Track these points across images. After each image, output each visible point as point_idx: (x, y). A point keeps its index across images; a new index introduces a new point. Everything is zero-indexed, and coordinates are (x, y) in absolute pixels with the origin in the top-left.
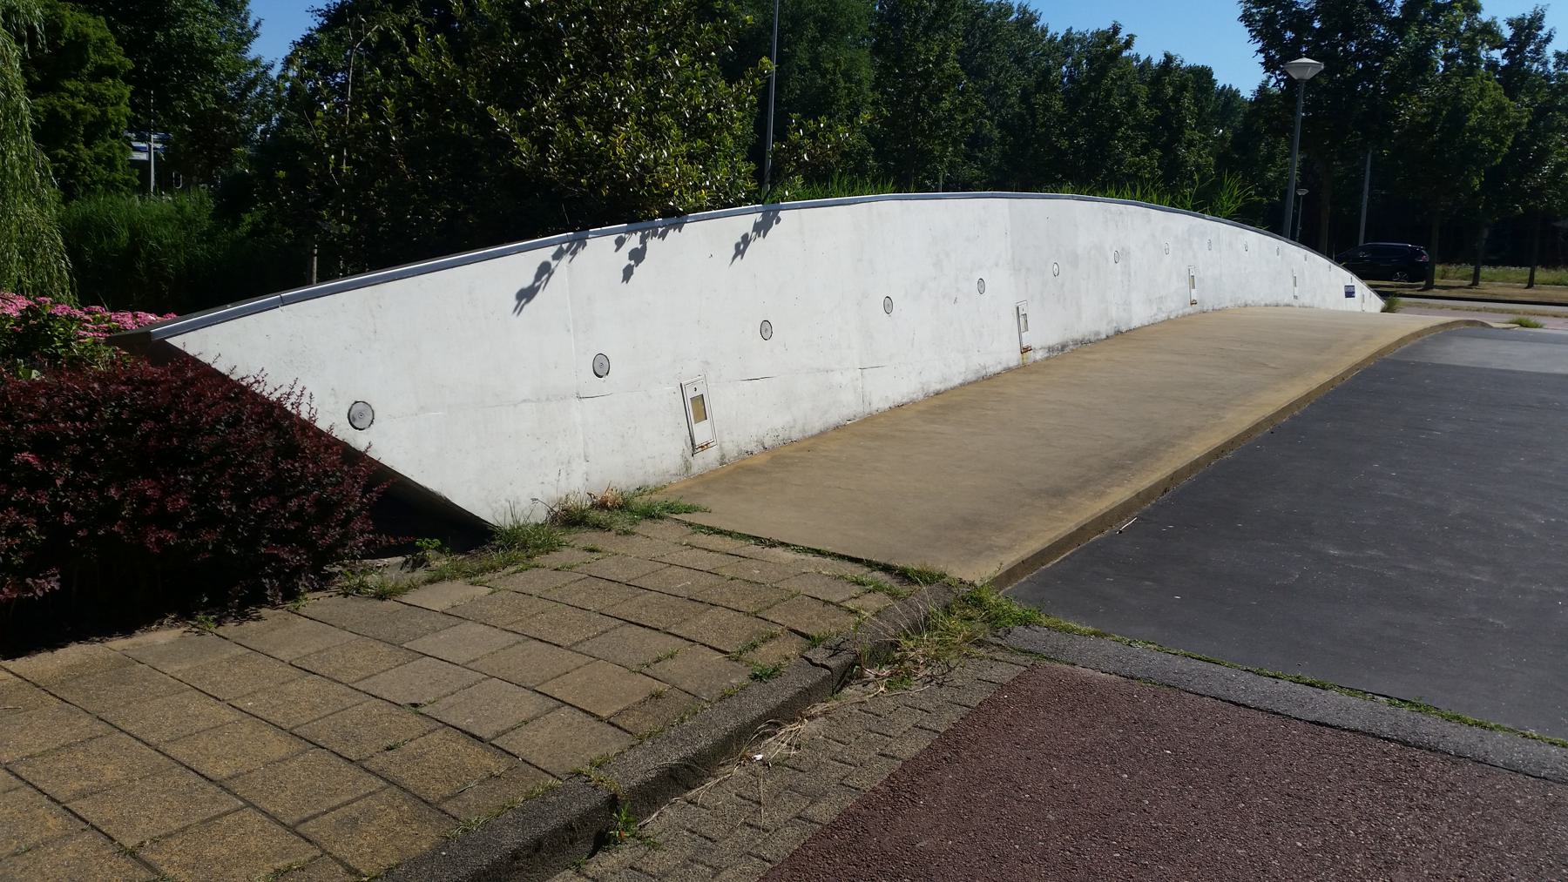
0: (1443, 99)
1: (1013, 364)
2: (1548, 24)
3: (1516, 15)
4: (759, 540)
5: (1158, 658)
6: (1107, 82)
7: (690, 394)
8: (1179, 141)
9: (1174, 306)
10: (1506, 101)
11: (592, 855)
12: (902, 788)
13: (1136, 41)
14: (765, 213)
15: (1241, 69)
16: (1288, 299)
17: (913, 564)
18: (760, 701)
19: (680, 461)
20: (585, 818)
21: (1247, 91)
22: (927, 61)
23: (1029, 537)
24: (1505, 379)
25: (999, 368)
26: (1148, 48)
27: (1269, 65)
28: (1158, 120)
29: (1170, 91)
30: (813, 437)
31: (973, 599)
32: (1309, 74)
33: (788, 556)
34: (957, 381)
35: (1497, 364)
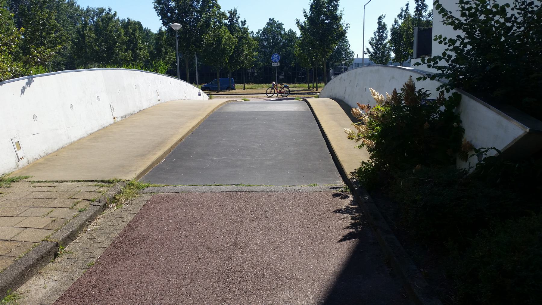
0: (215, 36)
1: (112, 123)
2: (238, 12)
3: (230, 10)
4: (57, 182)
5: (183, 188)
6: (109, 28)
7: (14, 141)
8: (136, 48)
9: (154, 102)
10: (231, 35)
11: (55, 259)
12: (132, 226)
13: (117, 14)
14: (29, 79)
15: (153, 23)
16: (184, 98)
17: (110, 178)
18: (84, 217)
19: (15, 164)
20: (52, 249)
21: (155, 30)
22: (43, 19)
23: (140, 167)
24: (245, 114)
25: (108, 125)
26: (122, 16)
27: (164, 24)
28: (129, 41)
29: (131, 30)
30: (55, 152)
31: (131, 184)
32: (178, 28)
33: (69, 184)
34: (96, 130)
35: (242, 110)
